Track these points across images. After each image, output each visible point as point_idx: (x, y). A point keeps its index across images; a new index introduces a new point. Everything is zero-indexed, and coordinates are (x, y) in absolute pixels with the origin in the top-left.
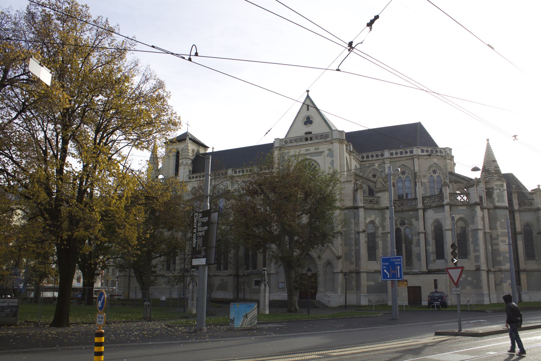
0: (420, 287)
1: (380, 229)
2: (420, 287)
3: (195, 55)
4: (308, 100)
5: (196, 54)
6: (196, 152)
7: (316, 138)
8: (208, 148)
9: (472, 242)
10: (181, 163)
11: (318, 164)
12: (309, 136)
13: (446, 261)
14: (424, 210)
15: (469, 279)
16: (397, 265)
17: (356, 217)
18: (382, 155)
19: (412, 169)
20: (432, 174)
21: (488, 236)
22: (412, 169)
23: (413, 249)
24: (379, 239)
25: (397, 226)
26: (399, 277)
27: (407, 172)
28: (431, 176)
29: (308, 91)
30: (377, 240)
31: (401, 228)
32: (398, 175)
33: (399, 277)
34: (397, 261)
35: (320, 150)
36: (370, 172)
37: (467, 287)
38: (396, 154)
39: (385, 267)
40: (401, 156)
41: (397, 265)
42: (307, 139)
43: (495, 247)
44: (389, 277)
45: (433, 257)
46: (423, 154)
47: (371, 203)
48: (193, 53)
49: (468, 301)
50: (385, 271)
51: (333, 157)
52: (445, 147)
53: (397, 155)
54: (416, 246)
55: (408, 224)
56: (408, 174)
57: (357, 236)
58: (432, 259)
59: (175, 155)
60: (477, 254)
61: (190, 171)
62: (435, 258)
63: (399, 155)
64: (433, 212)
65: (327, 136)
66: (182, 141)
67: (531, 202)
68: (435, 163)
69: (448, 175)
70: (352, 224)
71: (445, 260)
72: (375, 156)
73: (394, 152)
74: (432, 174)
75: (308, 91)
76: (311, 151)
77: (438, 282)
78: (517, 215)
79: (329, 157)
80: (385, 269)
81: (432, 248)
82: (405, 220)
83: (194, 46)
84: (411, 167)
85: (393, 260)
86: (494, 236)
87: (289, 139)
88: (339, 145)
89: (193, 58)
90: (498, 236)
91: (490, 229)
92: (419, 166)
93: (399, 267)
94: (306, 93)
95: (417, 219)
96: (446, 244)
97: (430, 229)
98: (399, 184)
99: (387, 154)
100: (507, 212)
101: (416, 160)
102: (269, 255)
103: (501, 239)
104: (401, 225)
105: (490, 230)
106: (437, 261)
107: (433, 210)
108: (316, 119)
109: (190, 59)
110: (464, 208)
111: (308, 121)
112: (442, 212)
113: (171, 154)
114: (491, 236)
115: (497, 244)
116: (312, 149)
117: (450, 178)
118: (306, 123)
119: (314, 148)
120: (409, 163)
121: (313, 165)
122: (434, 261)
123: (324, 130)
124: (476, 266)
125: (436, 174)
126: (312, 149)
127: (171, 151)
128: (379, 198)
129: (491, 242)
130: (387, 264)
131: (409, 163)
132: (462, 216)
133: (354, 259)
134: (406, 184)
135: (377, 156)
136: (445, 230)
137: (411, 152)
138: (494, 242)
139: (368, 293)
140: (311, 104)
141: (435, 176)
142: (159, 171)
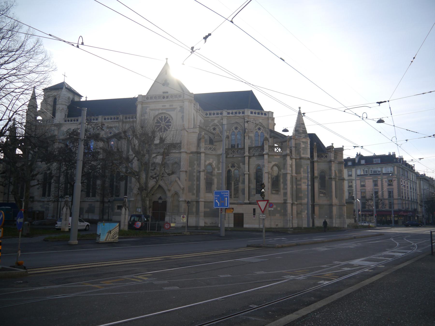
0: (242, 214)
1: (216, 170)
3: (81, 44)
5: (82, 44)
7: (172, 96)
9: (282, 183)
11: (172, 117)
12: (166, 95)
16: (225, 197)
24: (215, 177)
25: (229, 167)
26: (226, 205)
27: (239, 127)
28: (257, 132)
29: (167, 59)
33: (226, 205)
34: (225, 194)
37: (277, 215)
39: (216, 198)
41: (225, 197)
43: (298, 187)
44: (219, 205)
48: (80, 43)
49: (277, 225)
50: (217, 201)
62: (255, 193)
70: (195, 165)
75: (167, 59)
77: (256, 210)
78: (316, 165)
80: (217, 199)
83: (81, 37)
85: (223, 193)
86: (299, 178)
89: (80, 46)
90: (301, 178)
93: (226, 199)
98: (233, 137)
100: (309, 162)
104: (232, 167)
106: (256, 195)
109: (78, 47)
115: (300, 185)
122: (254, 195)
129: (296, 183)
130: (218, 196)
133: (195, 192)
134: (238, 137)
138: (298, 183)
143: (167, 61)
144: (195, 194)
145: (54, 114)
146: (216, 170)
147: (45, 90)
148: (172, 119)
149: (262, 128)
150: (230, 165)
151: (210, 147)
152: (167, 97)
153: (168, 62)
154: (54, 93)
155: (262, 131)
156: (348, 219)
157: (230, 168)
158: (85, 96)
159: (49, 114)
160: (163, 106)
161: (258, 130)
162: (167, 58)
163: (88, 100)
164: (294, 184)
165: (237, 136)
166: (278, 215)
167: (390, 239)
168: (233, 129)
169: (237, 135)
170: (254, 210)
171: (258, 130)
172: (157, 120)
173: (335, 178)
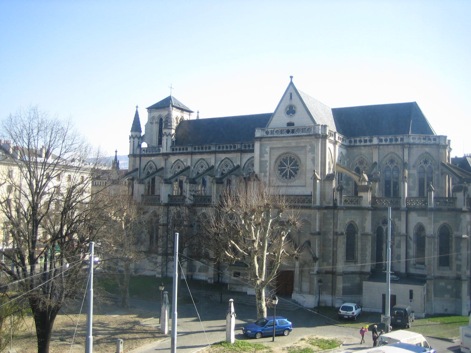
0: (395, 296)
2: (395, 296)
4: (291, 87)
6: (180, 119)
7: (298, 130)
8: (192, 112)
10: (164, 133)
11: (299, 159)
12: (291, 128)
15: (449, 287)
17: (335, 217)
28: (422, 167)
29: (291, 77)
31: (383, 227)
38: (386, 140)
42: (288, 132)
47: (352, 203)
49: (446, 310)
53: (386, 142)
54: (396, 247)
57: (335, 237)
60: (458, 263)
61: (173, 141)
65: (309, 129)
66: (166, 108)
70: (331, 225)
72: (363, 141)
73: (383, 138)
75: (291, 77)
77: (414, 292)
79: (311, 153)
84: (401, 156)
87: (270, 130)
95: (400, 220)
99: (375, 141)
108: (299, 108)
123: (307, 122)
127: (153, 118)
134: (394, 174)
135: (365, 141)
137: (402, 139)
139: (343, 294)
141: (426, 167)
142: (142, 139)
145: (160, 142)
148: (300, 162)
151: (352, 200)
152: (293, 131)
157: (381, 225)
158: (196, 111)
159: (155, 143)
161: (424, 164)
162: (291, 75)
163: (200, 118)
165: (394, 172)
166: (447, 296)
168: (388, 163)
169: (393, 172)
170: (411, 292)
171: (424, 164)
172: (281, 162)
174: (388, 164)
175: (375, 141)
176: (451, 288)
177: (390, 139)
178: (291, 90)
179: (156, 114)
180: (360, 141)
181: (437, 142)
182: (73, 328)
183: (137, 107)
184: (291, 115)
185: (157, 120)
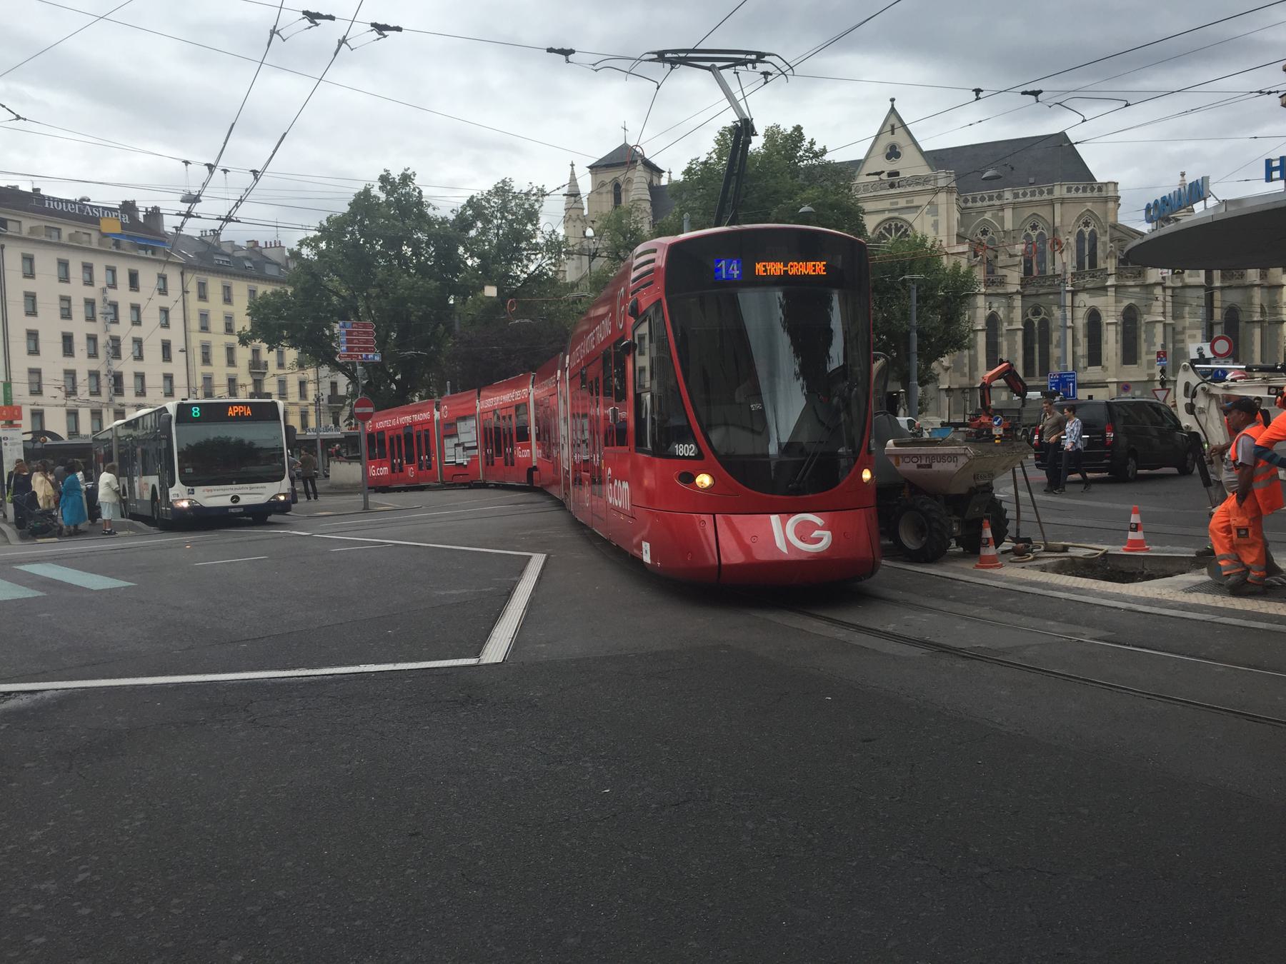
1: (1005, 324)
8: (664, 172)
9: (1145, 341)
13: (1105, 369)
14: (1074, 293)
16: (1070, 382)
18: (1000, 197)
19: (1050, 221)
20: (1082, 228)
21: (1169, 330)
22: (1050, 221)
23: (1051, 351)
24: (1003, 338)
25: (1027, 316)
27: (1041, 225)
28: (1081, 231)
29: (892, 100)
30: (1000, 339)
32: (1026, 231)
35: (915, 204)
36: (978, 225)
39: (1053, 385)
40: (1033, 199)
41: (1070, 382)
43: (1180, 345)
45: (1082, 363)
46: (1069, 195)
51: (937, 215)
52: (1106, 181)
55: (1045, 314)
56: (1043, 229)
58: (1081, 365)
59: (613, 190)
62: (1086, 364)
63: (1028, 198)
64: (1088, 296)
67: (1242, 273)
68: (1088, 210)
69: (1108, 229)
71: (1103, 367)
74: (1082, 228)
75: (892, 100)
76: (899, 206)
78: (1217, 295)
81: (1082, 350)
82: (1042, 308)
86: (1179, 329)
88: (947, 197)
90: (1184, 328)
91: (1174, 317)
92: (1062, 215)
94: (890, 103)
96: (1107, 343)
97: (1081, 322)
99: (1008, 195)
100: (1202, 293)
101: (1057, 207)
102: (860, 366)
103: (1188, 332)
104: (1033, 315)
105: (1173, 319)
106: (1089, 368)
107: (1087, 293)
110: (1137, 290)
111: (893, 153)
112: (1104, 296)
113: (604, 190)
114: (1174, 329)
115: (1183, 341)
116: (902, 203)
117: (1111, 235)
118: (889, 157)
119: (905, 200)
120: (1044, 212)
121: (902, 226)
122: (1085, 368)
124: (1148, 375)
125: (1083, 223)
126: (902, 203)
127: (603, 184)
128: (1005, 278)
129: (1173, 338)
131: (1044, 212)
132: (1133, 301)
133: (966, 370)
134: (1038, 246)
136: (1105, 324)
138: (1179, 337)
140: (897, 125)
143: (893, 105)
144: (968, 374)
146: (1005, 324)
147: (594, 169)
149: (1094, 222)
150: (1029, 312)
153: (895, 106)
154: (618, 174)
155: (1093, 229)
156: (756, 363)
157: (1030, 317)
160: (892, 204)
164: (1169, 339)
167: (1036, 323)
173: (1261, 321)
174: (1028, 231)
175: (1008, 195)
176: (1273, 173)
177: (976, 202)
178: (893, 120)
179: (608, 177)
180: (974, 200)
181: (1104, 194)
182: (989, 291)
183: (572, 165)
184: (893, 160)
185: (610, 188)
